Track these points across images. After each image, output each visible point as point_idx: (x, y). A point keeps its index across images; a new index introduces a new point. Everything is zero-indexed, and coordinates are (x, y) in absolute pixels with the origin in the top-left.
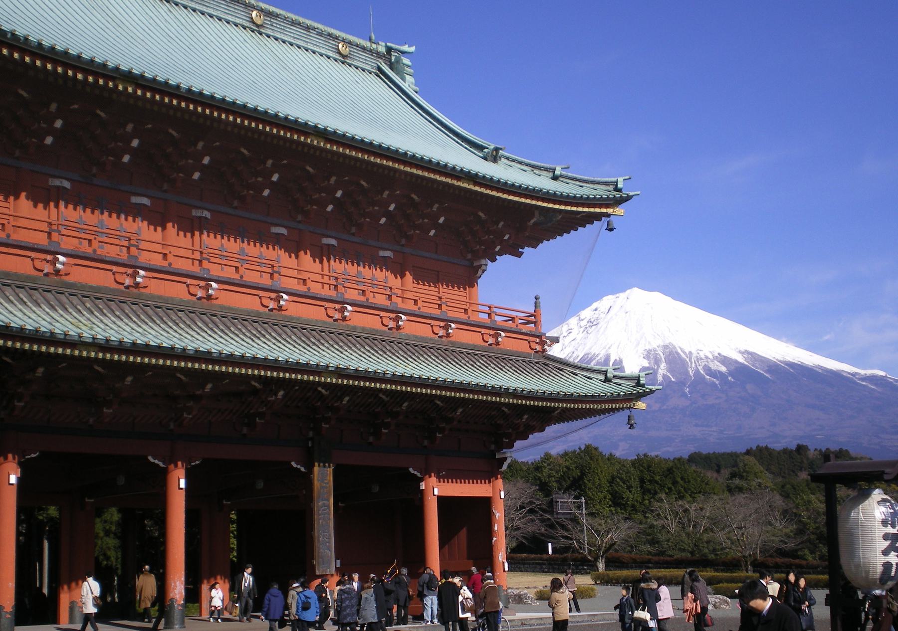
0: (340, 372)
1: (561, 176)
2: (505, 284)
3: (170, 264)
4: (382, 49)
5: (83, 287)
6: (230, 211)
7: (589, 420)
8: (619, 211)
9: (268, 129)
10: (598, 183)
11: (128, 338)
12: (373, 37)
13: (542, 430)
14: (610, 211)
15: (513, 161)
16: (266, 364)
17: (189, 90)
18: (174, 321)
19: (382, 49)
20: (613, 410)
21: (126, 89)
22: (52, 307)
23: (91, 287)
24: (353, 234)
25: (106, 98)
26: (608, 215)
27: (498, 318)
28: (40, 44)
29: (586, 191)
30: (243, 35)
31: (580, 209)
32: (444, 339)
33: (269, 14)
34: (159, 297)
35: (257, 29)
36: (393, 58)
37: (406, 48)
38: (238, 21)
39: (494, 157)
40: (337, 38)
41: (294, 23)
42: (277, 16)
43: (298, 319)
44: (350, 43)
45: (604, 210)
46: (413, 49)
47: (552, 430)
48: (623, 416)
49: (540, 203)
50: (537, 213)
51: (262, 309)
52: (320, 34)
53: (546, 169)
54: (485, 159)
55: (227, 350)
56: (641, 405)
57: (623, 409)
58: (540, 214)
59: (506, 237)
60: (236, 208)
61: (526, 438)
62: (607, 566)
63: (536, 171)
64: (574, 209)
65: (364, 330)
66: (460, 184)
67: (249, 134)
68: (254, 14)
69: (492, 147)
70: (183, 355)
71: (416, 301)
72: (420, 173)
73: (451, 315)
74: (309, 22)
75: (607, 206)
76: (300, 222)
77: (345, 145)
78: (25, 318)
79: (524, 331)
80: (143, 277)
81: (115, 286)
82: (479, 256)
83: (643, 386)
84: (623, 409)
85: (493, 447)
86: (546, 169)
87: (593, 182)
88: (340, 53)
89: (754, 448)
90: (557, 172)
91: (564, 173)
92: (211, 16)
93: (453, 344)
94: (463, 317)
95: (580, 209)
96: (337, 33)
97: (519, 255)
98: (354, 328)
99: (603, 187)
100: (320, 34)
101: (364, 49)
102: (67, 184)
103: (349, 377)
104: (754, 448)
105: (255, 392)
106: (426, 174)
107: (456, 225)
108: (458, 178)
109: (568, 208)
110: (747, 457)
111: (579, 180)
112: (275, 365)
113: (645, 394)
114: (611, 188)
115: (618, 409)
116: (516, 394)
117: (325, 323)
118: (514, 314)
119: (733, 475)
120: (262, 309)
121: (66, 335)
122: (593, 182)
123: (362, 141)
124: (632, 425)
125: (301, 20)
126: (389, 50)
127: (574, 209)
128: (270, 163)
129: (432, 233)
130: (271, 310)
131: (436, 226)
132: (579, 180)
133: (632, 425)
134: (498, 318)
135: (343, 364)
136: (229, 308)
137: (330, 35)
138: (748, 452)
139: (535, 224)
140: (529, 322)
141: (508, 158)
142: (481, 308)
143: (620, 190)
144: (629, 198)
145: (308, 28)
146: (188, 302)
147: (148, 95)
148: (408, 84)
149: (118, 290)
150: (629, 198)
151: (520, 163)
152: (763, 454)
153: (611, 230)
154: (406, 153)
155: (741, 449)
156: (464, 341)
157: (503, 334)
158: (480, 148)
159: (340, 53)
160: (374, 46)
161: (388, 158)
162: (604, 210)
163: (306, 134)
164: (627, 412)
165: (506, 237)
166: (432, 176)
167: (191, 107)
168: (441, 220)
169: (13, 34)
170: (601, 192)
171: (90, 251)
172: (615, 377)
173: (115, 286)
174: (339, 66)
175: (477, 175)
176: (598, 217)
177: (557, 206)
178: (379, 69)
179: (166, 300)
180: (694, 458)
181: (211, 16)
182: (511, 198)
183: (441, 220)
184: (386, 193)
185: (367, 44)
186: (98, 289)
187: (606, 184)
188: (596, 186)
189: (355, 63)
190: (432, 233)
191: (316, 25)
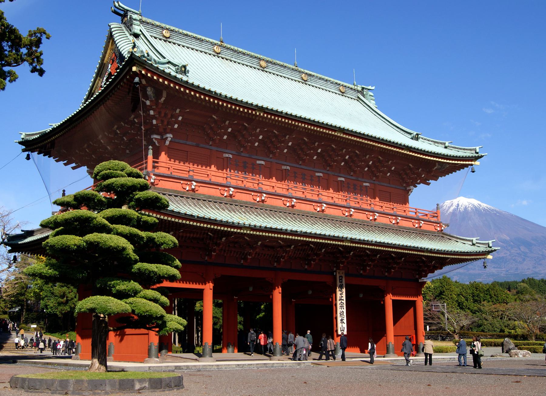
0: (352, 241)
1: (448, 146)
2: (422, 197)
3: (210, 180)
4: (360, 89)
5: (241, 202)
6: (298, 166)
7: (463, 264)
8: (477, 163)
9: (276, 118)
10: (467, 149)
11: (264, 225)
12: (355, 83)
13: (441, 268)
14: (473, 163)
15: (425, 139)
16: (316, 236)
17: (286, 114)
18: (278, 217)
19: (360, 89)
20: (476, 259)
21: (260, 114)
22: (229, 211)
23: (244, 202)
24: (352, 176)
25: (250, 119)
26: (472, 165)
27: (419, 215)
28: (226, 96)
29: (461, 154)
30: (201, 57)
31: (459, 162)
32: (395, 225)
33: (310, 75)
34: (271, 206)
35: (305, 82)
36: (365, 93)
37: (370, 87)
38: (296, 79)
39: (416, 138)
40: (339, 84)
41: (320, 79)
42: (313, 76)
43: (330, 215)
44: (345, 86)
45: (470, 163)
46: (373, 88)
47: (446, 268)
48: (479, 263)
49: (440, 160)
50: (437, 164)
51: (314, 211)
52: (332, 83)
53: (441, 143)
54: (412, 139)
55: (304, 230)
56: (490, 257)
57: (480, 259)
58: (439, 165)
59: (423, 176)
60: (300, 165)
61: (433, 272)
62: (460, 338)
63: (436, 144)
64: (456, 162)
65: (359, 220)
66: (403, 151)
67: (274, 122)
68: (215, 48)
69: (415, 133)
70: (285, 232)
71: (332, 198)
72: (385, 147)
73: (399, 213)
74: (326, 78)
75: (472, 161)
76: (300, 165)
77: (324, 128)
78: (206, 212)
79: (432, 221)
80: (233, 192)
81: (253, 201)
82: (408, 185)
83: (491, 247)
84: (480, 259)
85: (417, 276)
86: (441, 143)
87: (464, 149)
88: (341, 91)
89: (526, 279)
90: (447, 144)
91: (450, 145)
92: (285, 77)
93: (400, 227)
94: (404, 214)
95: (459, 162)
96: (339, 82)
97: (428, 184)
98: (355, 220)
99: (469, 151)
100: (332, 83)
101: (351, 89)
102: (231, 156)
103: (356, 243)
104: (526, 279)
105: (368, 255)
106: (358, 140)
107: (395, 171)
108: (402, 149)
109: (453, 162)
110: (522, 284)
111: (457, 148)
112: (324, 237)
113: (492, 251)
114: (473, 152)
115: (478, 259)
116: (431, 251)
117: (342, 217)
118: (427, 213)
119: (518, 293)
120: (314, 211)
121: (239, 224)
122: (464, 149)
123: (323, 123)
124: (485, 267)
125: (323, 77)
126: (363, 88)
127: (456, 162)
128: (258, 130)
129: (389, 174)
130: (318, 212)
131: (390, 171)
132: (457, 148)
133: (485, 267)
134: (419, 215)
135: (354, 237)
136: (300, 211)
137: (336, 83)
138: (523, 281)
139: (436, 169)
140: (434, 217)
141: (422, 138)
142: (410, 209)
143: (477, 153)
144: (482, 156)
145: (327, 80)
146: (283, 208)
147: (246, 110)
148: (372, 104)
149: (254, 203)
150: (482, 156)
151: (428, 140)
152: (531, 282)
153: (473, 172)
154: (379, 138)
155: (519, 279)
156: (404, 225)
157: (423, 222)
158: (410, 134)
159: (341, 91)
160: (356, 87)
161: (352, 135)
162: (470, 163)
163: (335, 131)
164: (483, 260)
165: (423, 176)
166: (390, 148)
167: (273, 117)
168: (393, 168)
169: (215, 93)
170: (468, 154)
171: (243, 186)
172: (477, 243)
173: (253, 201)
174: (340, 97)
175: (411, 147)
176: (467, 166)
177: (448, 161)
178: (358, 97)
179: (275, 207)
180: (495, 284)
181: (285, 77)
182: (427, 157)
183: (393, 168)
184: (368, 156)
185: (353, 86)
186: (246, 203)
187: (470, 150)
188: (465, 151)
189: (348, 95)
190: (389, 174)
191: (329, 79)
